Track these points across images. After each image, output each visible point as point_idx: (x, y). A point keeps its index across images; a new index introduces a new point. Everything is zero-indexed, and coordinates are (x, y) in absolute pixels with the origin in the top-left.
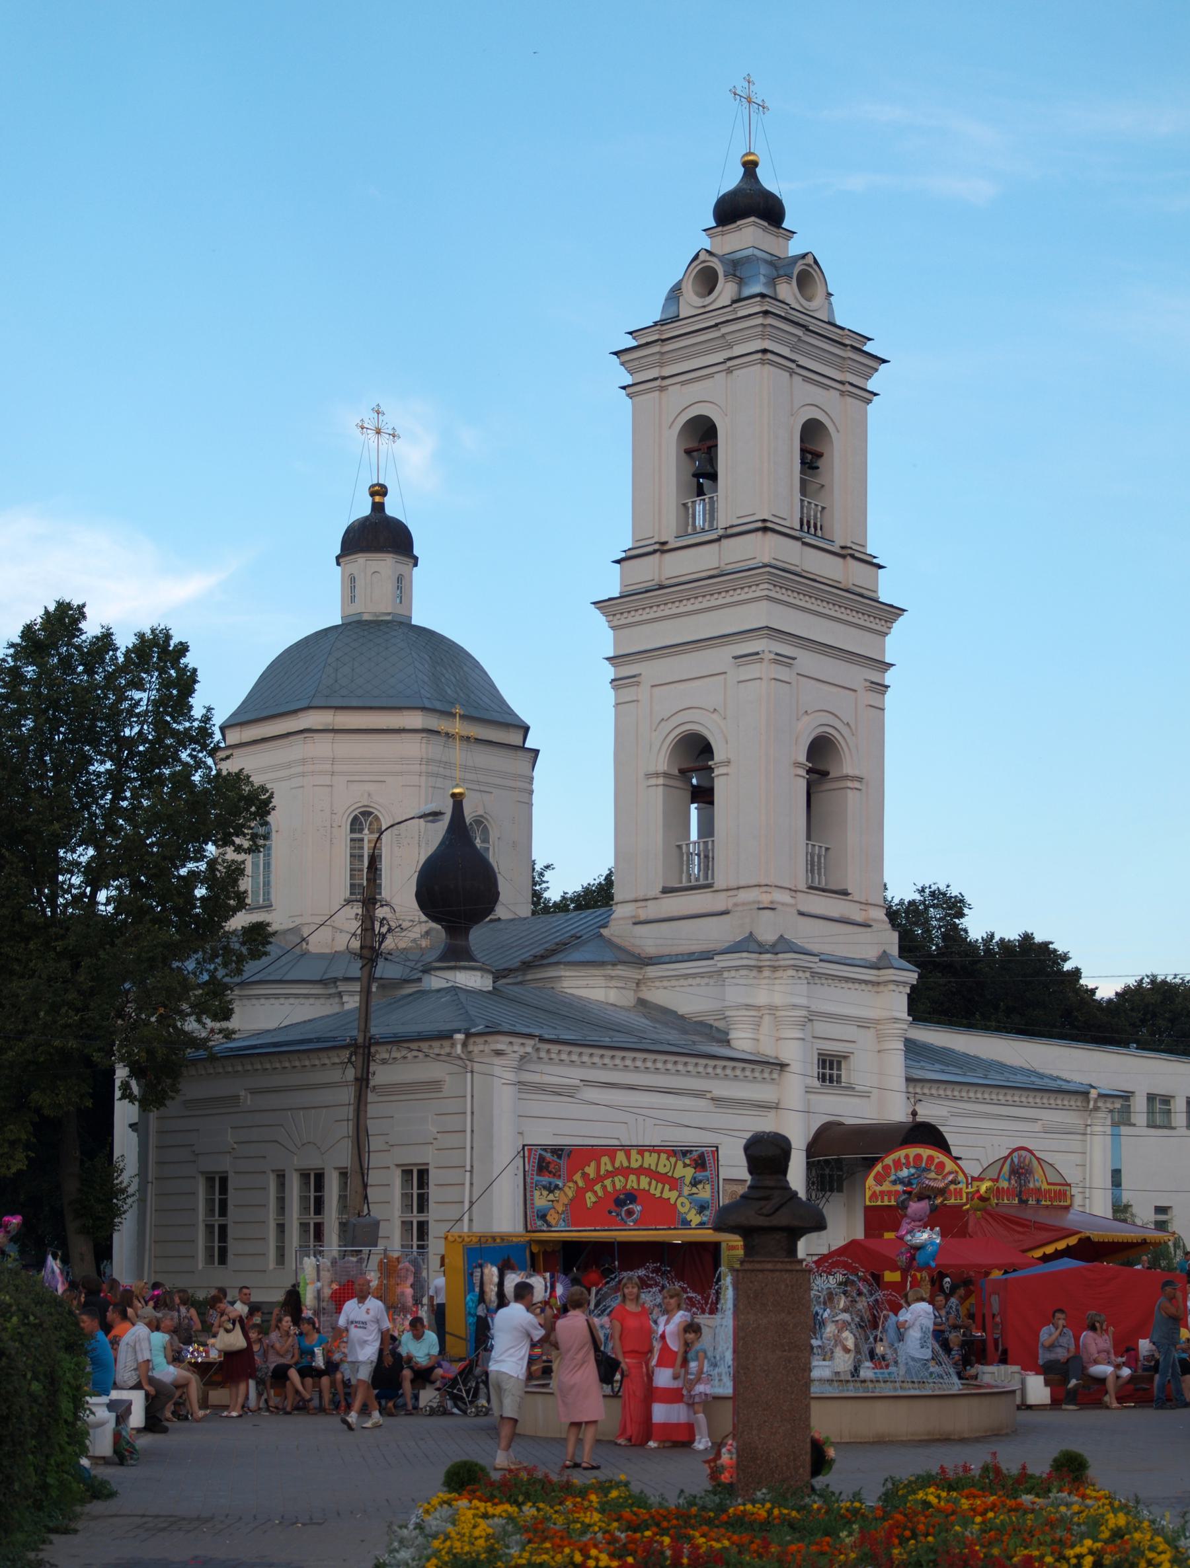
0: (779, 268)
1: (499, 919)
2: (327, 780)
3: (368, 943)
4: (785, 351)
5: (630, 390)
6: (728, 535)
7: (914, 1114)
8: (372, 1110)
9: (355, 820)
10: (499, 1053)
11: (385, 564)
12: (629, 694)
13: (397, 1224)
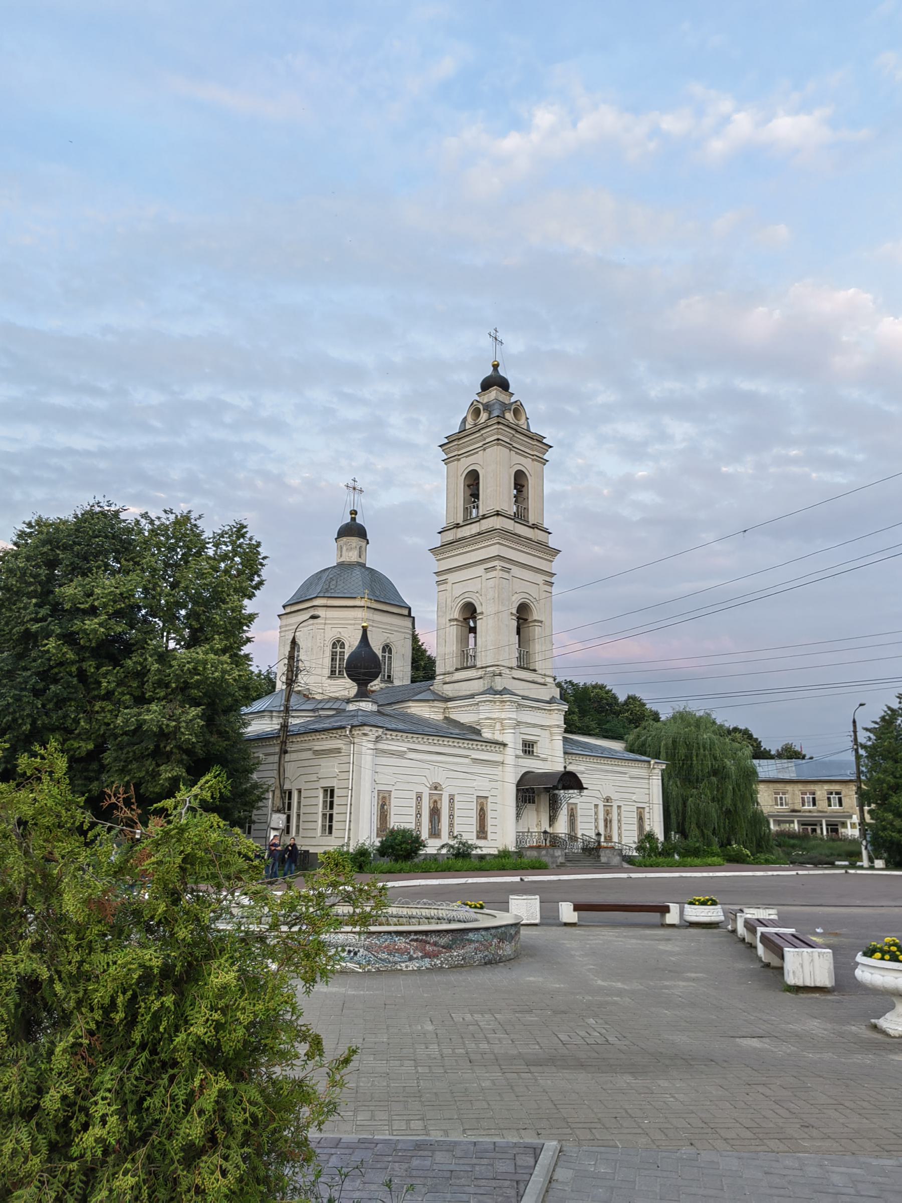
0: (505, 407)
2: (322, 626)
3: (290, 677)
6: (484, 517)
7: (565, 767)
9: (334, 644)
10: (365, 735)
11: (355, 541)
12: (442, 587)
13: (320, 814)
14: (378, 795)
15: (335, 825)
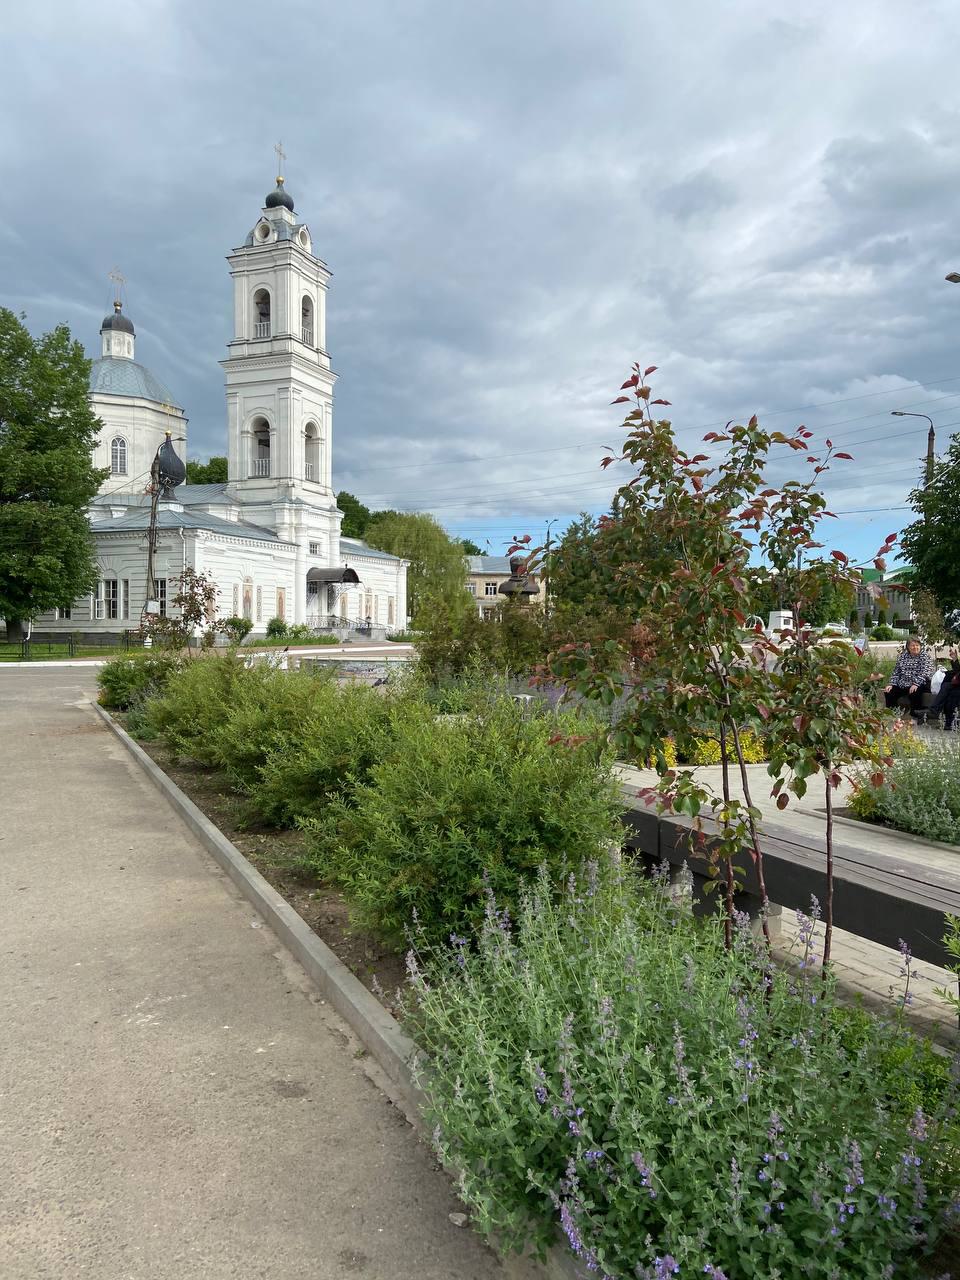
4: (297, 265)
6: (275, 339)
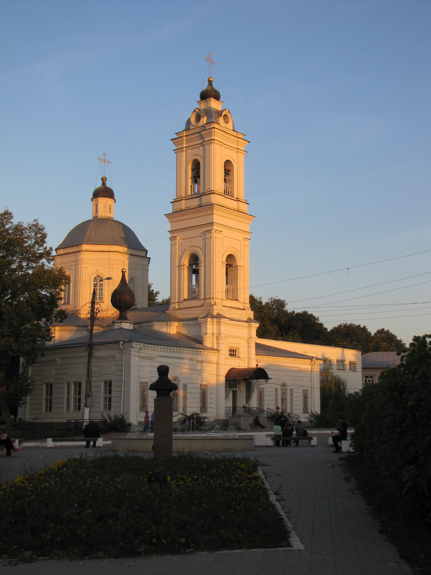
1: (137, 308)
5: (176, 151)
7: (257, 365)
8: (93, 364)
13: (102, 398)
14: (140, 385)
15: (113, 404)
